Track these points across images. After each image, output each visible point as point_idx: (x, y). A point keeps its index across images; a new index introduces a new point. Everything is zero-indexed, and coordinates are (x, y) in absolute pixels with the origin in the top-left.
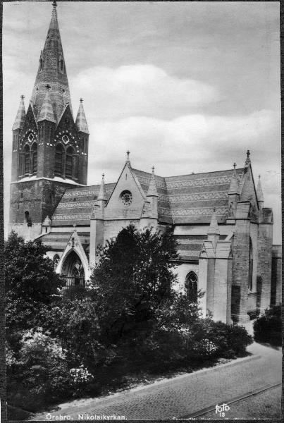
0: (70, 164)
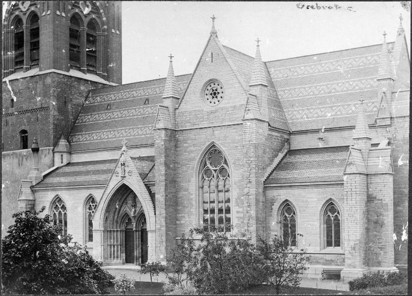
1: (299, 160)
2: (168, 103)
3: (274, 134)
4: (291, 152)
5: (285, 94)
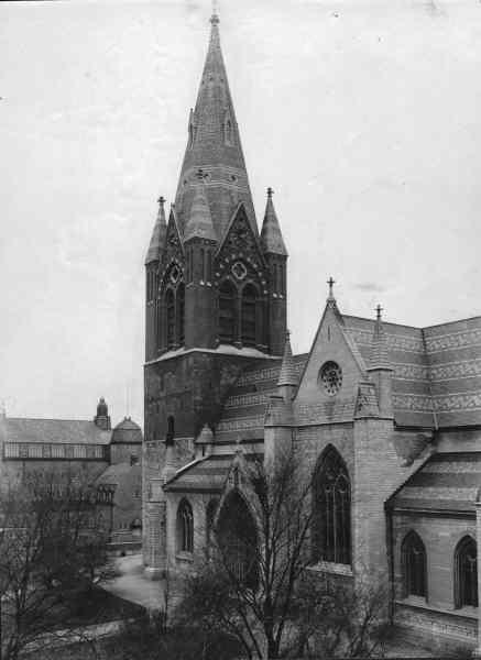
0: (251, 319)
1: (440, 471)
2: (282, 392)
3: (405, 434)
4: (438, 458)
5: (439, 373)
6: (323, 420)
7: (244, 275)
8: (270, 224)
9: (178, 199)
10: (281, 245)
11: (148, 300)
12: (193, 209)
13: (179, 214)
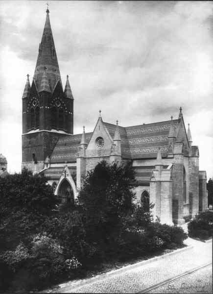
6: (97, 156)
7: (59, 105)
8: (68, 88)
9: (35, 76)
10: (72, 96)
11: (23, 111)
12: (42, 81)
13: (36, 81)
